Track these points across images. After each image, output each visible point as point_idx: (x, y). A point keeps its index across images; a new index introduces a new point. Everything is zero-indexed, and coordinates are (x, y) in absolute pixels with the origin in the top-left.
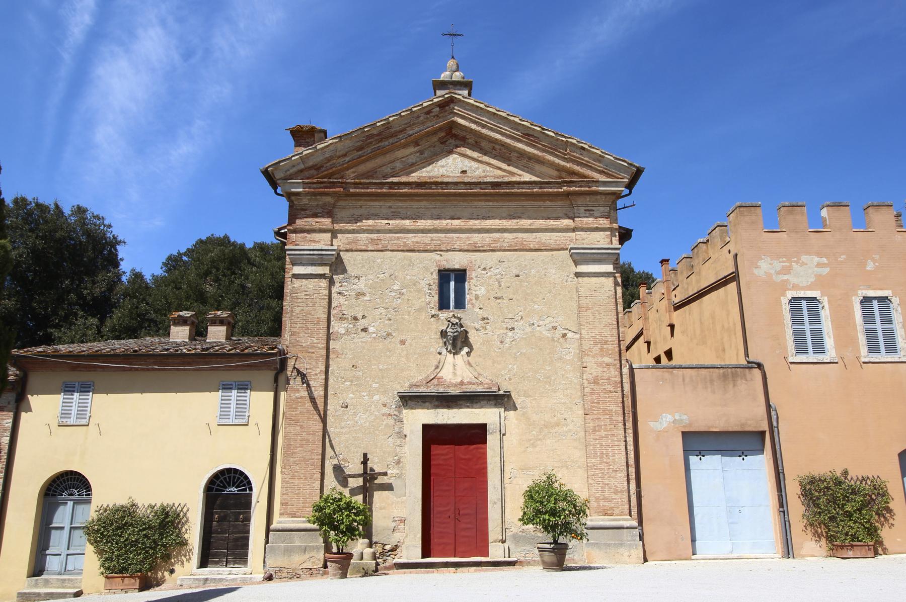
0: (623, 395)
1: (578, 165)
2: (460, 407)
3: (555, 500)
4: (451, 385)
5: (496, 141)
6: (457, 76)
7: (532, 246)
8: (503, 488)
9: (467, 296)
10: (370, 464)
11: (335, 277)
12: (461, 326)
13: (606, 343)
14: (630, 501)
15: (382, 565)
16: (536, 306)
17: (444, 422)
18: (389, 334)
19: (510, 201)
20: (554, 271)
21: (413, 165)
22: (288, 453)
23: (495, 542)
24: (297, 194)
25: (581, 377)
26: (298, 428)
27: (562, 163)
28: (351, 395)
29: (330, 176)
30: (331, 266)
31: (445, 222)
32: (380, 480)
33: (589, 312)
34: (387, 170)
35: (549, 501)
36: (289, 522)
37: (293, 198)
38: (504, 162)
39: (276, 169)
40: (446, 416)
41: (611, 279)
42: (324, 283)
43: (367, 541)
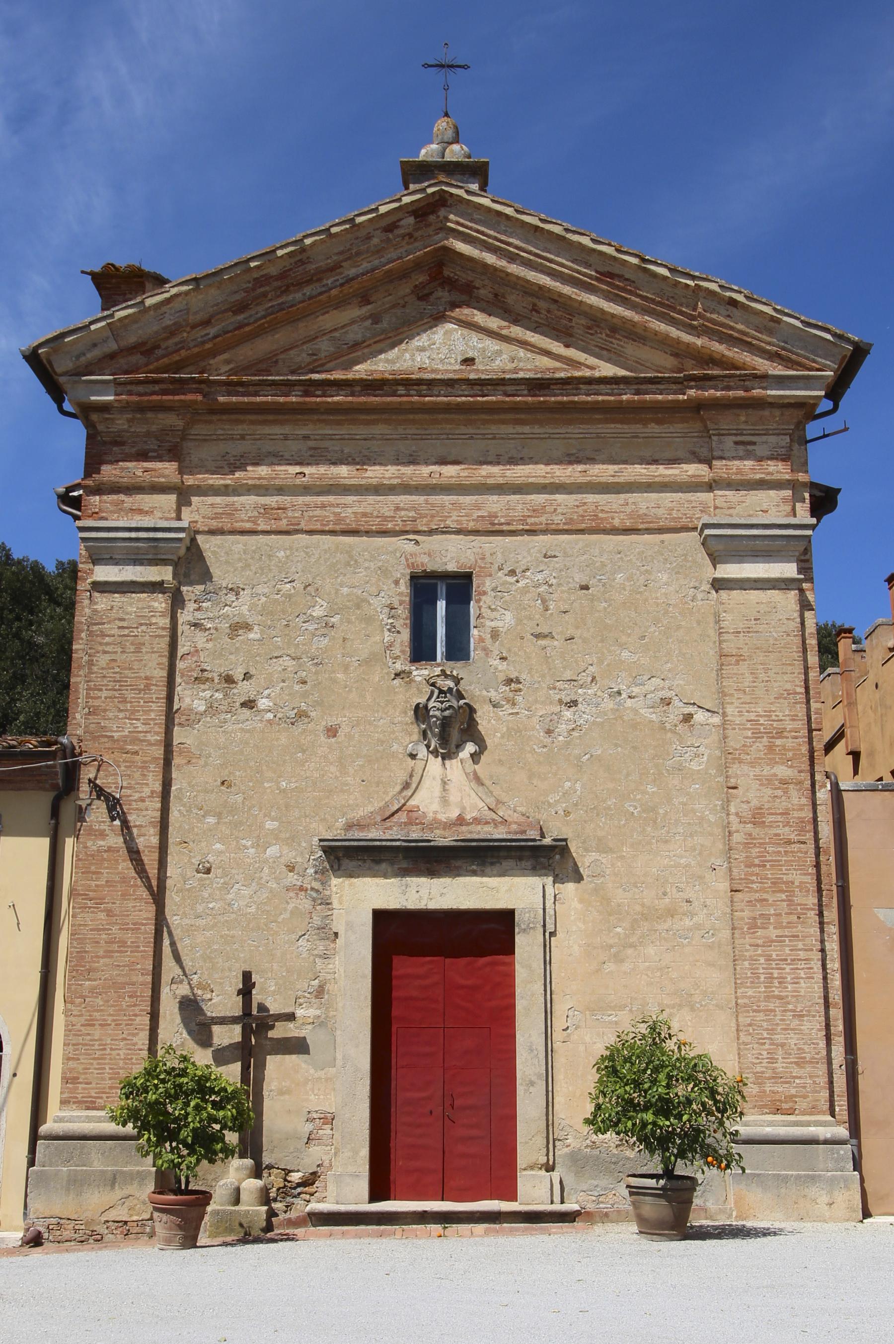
0: (818, 848)
1: (720, 342)
2: (455, 872)
3: (669, 1077)
4: (436, 824)
5: (540, 291)
6: (456, 152)
7: (617, 523)
8: (549, 1051)
9: (474, 632)
10: (257, 996)
11: (184, 589)
12: (460, 696)
13: (780, 734)
14: (831, 1083)
15: (282, 1216)
16: (625, 654)
17: (421, 905)
18: (301, 715)
19: (570, 422)
20: (665, 577)
21: (356, 346)
22: (78, 969)
23: (532, 1168)
24: (104, 408)
25: (725, 809)
26: (102, 916)
27: (686, 338)
28: (218, 846)
29: (178, 367)
30: (176, 564)
31: (425, 470)
32: (279, 1031)
33: (743, 668)
34: (301, 357)
35: (654, 1082)
36: (79, 1119)
37: (94, 417)
38: (557, 339)
39: (55, 350)
40: (424, 893)
41: (793, 594)
42: (160, 603)
43: (249, 1162)
